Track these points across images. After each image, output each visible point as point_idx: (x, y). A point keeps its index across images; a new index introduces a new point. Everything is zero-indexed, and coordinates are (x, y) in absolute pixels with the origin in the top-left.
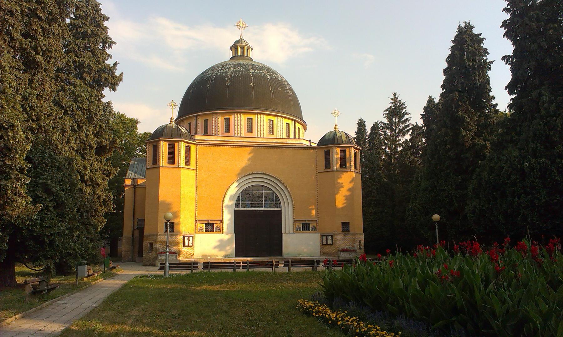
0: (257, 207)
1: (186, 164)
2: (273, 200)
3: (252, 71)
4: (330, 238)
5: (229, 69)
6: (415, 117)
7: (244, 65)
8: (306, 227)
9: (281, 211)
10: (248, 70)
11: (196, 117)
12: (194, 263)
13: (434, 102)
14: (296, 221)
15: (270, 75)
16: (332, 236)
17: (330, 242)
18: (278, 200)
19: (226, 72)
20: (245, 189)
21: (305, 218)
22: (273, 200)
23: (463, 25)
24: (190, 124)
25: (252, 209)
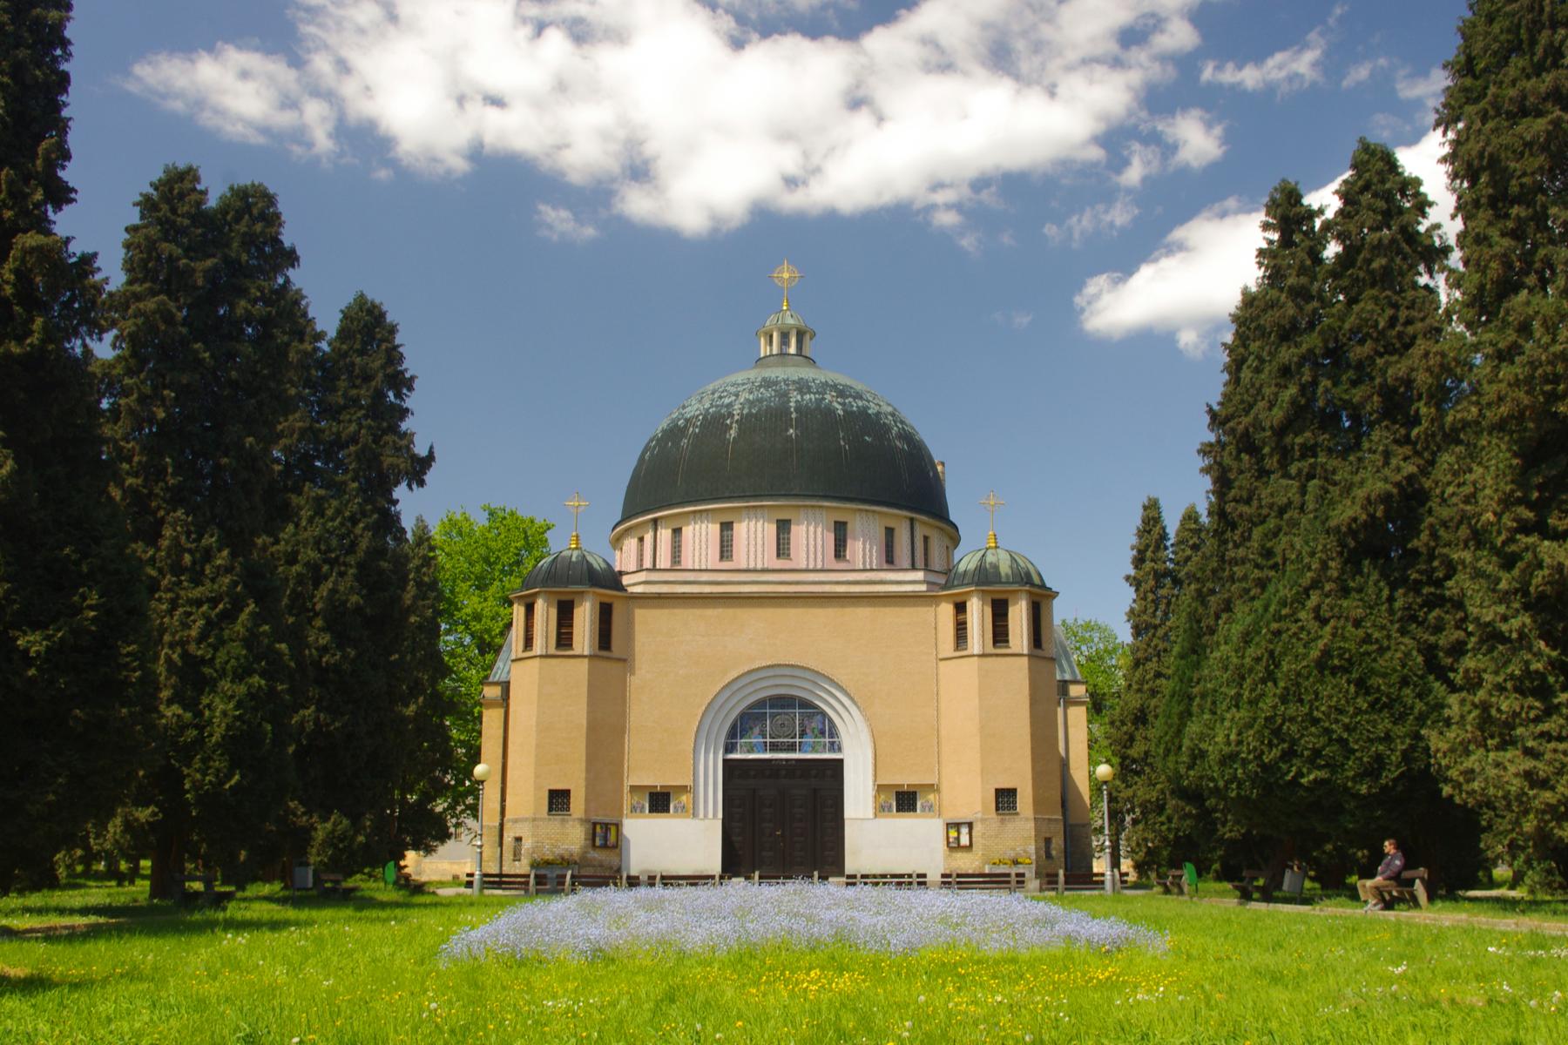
0: (782, 750)
1: (995, 642)
2: (822, 733)
3: (795, 397)
4: (964, 830)
5: (737, 395)
6: (1204, 519)
7: (776, 383)
8: (906, 800)
9: (841, 761)
10: (784, 395)
11: (655, 521)
12: (919, 876)
13: (381, 463)
14: (880, 788)
15: (843, 404)
16: (970, 825)
17: (965, 840)
18: (833, 732)
19: (730, 405)
20: (751, 707)
21: (906, 779)
22: (822, 733)
23: (73, 195)
24: (641, 540)
25: (767, 756)
